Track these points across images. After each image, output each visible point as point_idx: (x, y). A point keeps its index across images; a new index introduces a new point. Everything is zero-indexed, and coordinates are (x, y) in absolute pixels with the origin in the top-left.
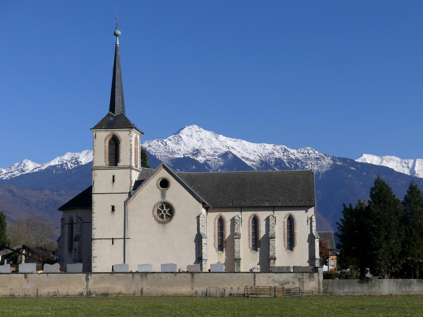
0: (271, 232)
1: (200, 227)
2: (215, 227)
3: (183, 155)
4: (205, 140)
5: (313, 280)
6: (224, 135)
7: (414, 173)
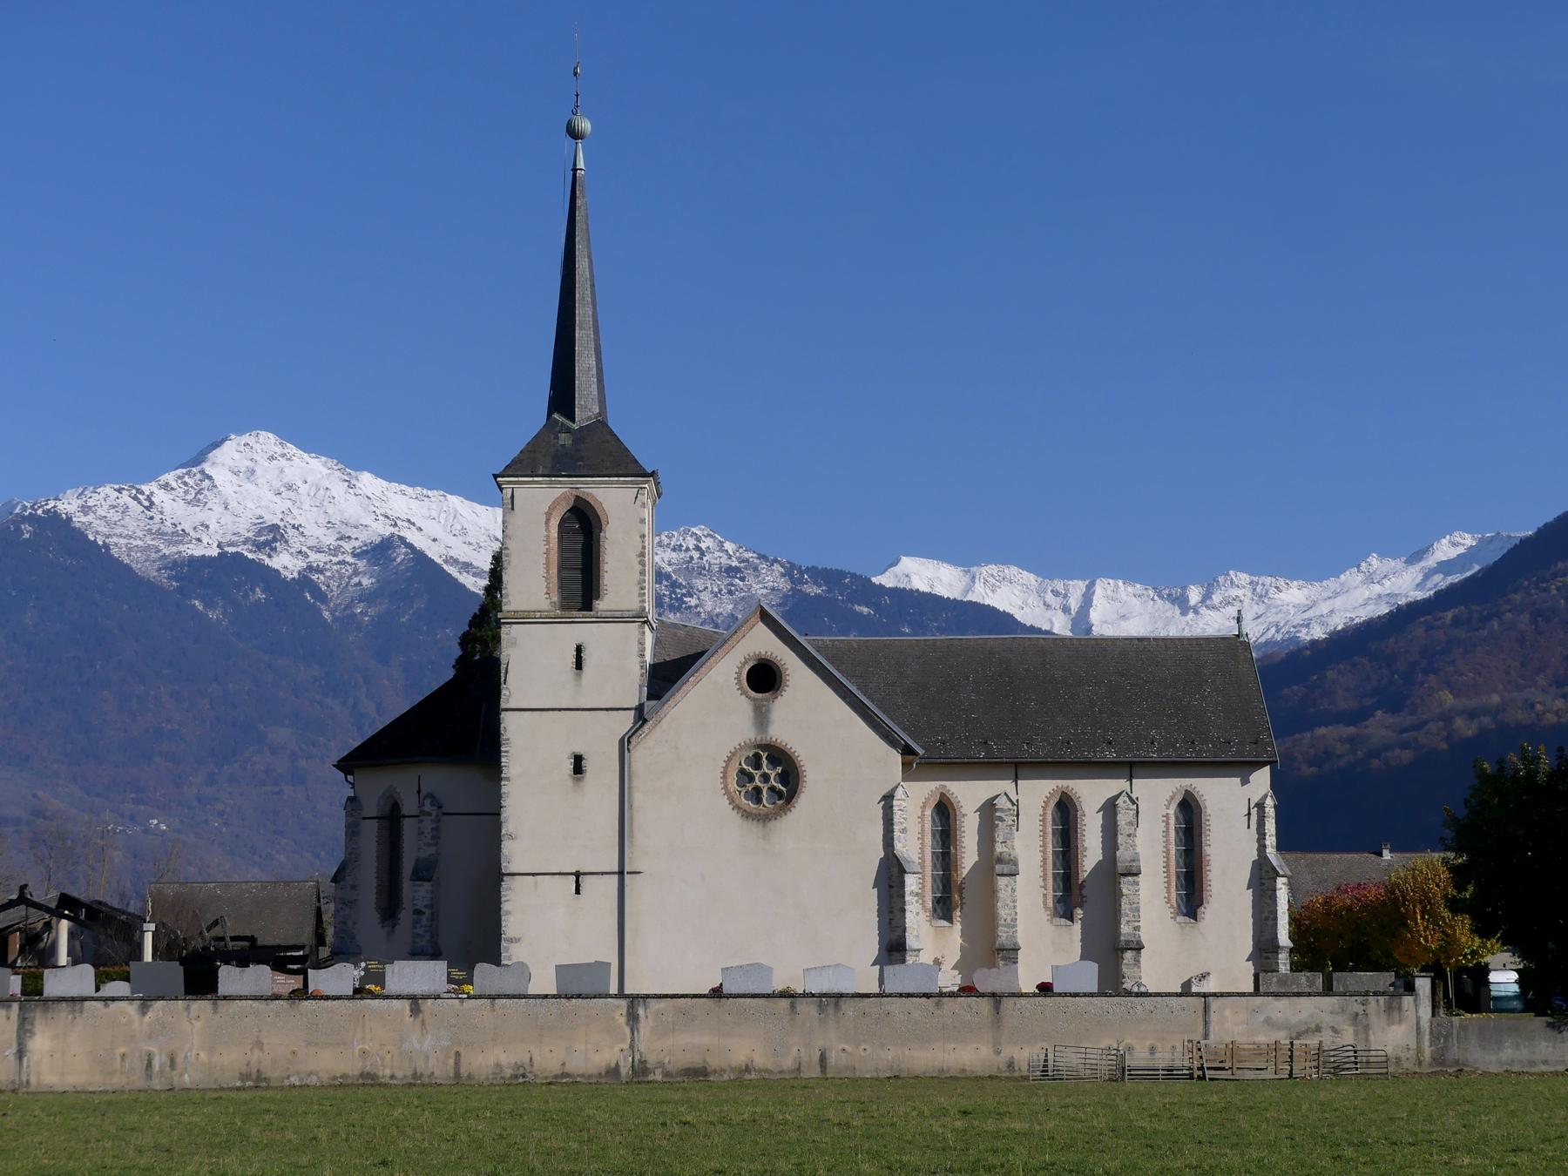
0: (1123, 854)
1: (896, 834)
2: (922, 832)
3: (219, 546)
4: (303, 489)
5: (1400, 1021)
6: (378, 474)
7: (1089, 630)
